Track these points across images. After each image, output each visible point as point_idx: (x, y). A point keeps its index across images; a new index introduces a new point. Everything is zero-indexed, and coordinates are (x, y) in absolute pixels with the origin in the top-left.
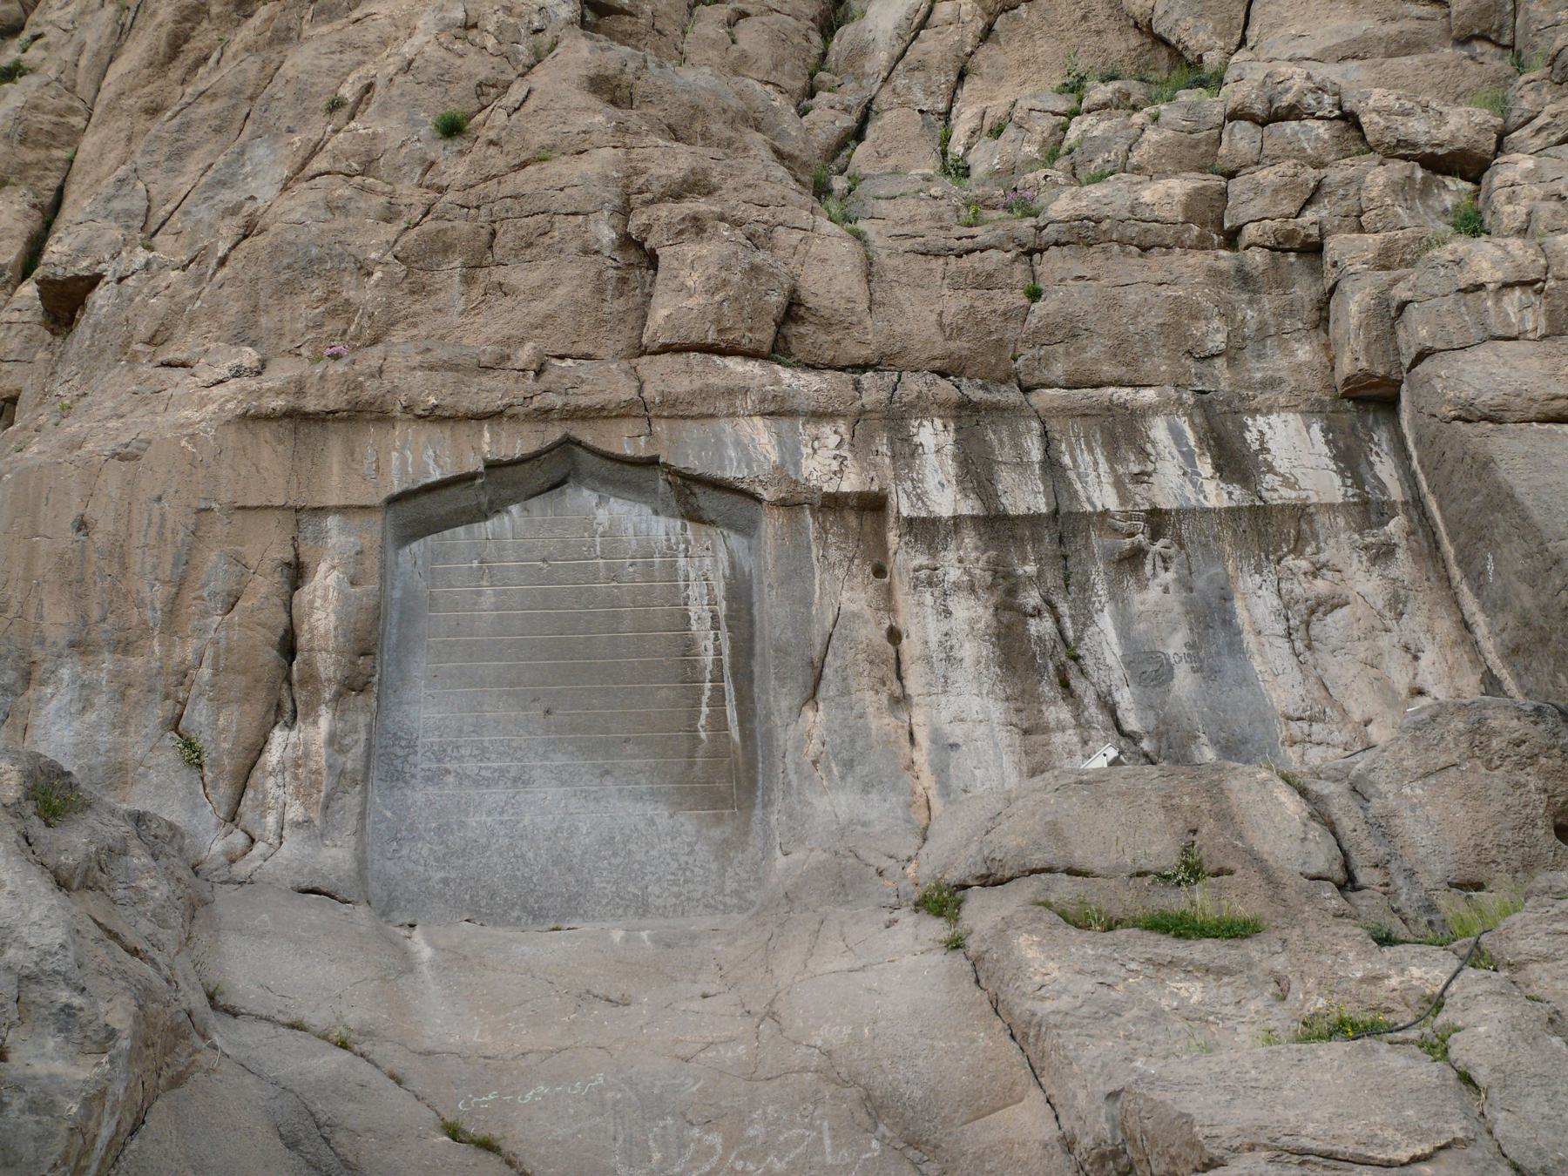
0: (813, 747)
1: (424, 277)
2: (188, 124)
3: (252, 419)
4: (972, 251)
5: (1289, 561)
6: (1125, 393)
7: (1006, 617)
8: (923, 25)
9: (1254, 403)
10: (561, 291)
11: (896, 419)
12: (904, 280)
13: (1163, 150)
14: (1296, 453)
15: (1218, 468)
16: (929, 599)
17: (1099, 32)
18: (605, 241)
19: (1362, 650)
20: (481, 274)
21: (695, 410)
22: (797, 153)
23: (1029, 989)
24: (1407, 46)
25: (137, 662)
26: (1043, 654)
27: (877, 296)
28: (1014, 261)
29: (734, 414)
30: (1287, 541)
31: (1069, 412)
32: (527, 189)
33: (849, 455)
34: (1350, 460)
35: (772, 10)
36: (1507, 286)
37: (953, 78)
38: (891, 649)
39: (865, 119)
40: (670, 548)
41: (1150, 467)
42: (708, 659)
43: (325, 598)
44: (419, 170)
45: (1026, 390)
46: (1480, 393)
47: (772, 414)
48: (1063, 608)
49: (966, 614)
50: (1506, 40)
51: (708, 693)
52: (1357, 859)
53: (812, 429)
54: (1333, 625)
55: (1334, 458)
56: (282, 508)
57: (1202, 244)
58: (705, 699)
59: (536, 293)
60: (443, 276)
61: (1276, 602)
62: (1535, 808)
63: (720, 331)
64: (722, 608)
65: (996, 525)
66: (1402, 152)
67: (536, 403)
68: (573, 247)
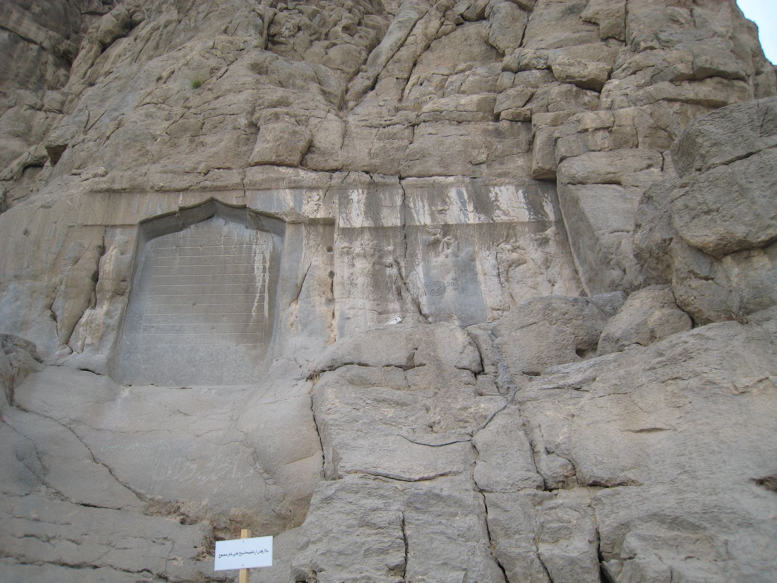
0: (292, 318)
1: (176, 141)
2: (109, 89)
3: (93, 192)
4: (390, 125)
5: (502, 245)
6: (441, 179)
7: (377, 267)
8: (402, 45)
9: (495, 182)
10: (222, 144)
11: (343, 191)
12: (359, 137)
13: (474, 84)
14: (510, 201)
15: (475, 208)
16: (346, 260)
17: (470, 45)
18: (243, 124)
19: (530, 282)
20: (196, 138)
21: (263, 187)
22: (333, 91)
23: (324, 410)
24: (581, 42)
25: (38, 283)
26: (391, 282)
27: (346, 143)
28: (405, 129)
29: (278, 188)
30: (502, 237)
31: (415, 186)
32: (218, 106)
33: (322, 204)
34: (535, 207)
35: (346, 43)
36: (597, 129)
37: (411, 65)
38: (329, 280)
39: (375, 82)
40: (250, 241)
41: (447, 207)
42: (259, 285)
43: (110, 259)
44: (182, 101)
45: (401, 178)
46: (578, 172)
47: (293, 188)
48: (402, 264)
49: (361, 266)
50: (622, 38)
51: (258, 298)
52: (486, 362)
53: (309, 194)
54: (517, 272)
55: (527, 204)
56: (100, 225)
57: (483, 119)
58: (256, 300)
59: (214, 144)
60: (183, 140)
61: (494, 262)
62: (568, 341)
63: (277, 156)
64: (267, 265)
65: (379, 231)
66: (568, 80)
67: (201, 185)
68: (230, 127)
